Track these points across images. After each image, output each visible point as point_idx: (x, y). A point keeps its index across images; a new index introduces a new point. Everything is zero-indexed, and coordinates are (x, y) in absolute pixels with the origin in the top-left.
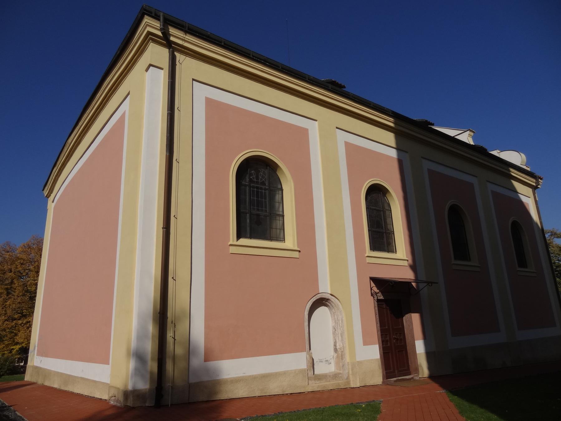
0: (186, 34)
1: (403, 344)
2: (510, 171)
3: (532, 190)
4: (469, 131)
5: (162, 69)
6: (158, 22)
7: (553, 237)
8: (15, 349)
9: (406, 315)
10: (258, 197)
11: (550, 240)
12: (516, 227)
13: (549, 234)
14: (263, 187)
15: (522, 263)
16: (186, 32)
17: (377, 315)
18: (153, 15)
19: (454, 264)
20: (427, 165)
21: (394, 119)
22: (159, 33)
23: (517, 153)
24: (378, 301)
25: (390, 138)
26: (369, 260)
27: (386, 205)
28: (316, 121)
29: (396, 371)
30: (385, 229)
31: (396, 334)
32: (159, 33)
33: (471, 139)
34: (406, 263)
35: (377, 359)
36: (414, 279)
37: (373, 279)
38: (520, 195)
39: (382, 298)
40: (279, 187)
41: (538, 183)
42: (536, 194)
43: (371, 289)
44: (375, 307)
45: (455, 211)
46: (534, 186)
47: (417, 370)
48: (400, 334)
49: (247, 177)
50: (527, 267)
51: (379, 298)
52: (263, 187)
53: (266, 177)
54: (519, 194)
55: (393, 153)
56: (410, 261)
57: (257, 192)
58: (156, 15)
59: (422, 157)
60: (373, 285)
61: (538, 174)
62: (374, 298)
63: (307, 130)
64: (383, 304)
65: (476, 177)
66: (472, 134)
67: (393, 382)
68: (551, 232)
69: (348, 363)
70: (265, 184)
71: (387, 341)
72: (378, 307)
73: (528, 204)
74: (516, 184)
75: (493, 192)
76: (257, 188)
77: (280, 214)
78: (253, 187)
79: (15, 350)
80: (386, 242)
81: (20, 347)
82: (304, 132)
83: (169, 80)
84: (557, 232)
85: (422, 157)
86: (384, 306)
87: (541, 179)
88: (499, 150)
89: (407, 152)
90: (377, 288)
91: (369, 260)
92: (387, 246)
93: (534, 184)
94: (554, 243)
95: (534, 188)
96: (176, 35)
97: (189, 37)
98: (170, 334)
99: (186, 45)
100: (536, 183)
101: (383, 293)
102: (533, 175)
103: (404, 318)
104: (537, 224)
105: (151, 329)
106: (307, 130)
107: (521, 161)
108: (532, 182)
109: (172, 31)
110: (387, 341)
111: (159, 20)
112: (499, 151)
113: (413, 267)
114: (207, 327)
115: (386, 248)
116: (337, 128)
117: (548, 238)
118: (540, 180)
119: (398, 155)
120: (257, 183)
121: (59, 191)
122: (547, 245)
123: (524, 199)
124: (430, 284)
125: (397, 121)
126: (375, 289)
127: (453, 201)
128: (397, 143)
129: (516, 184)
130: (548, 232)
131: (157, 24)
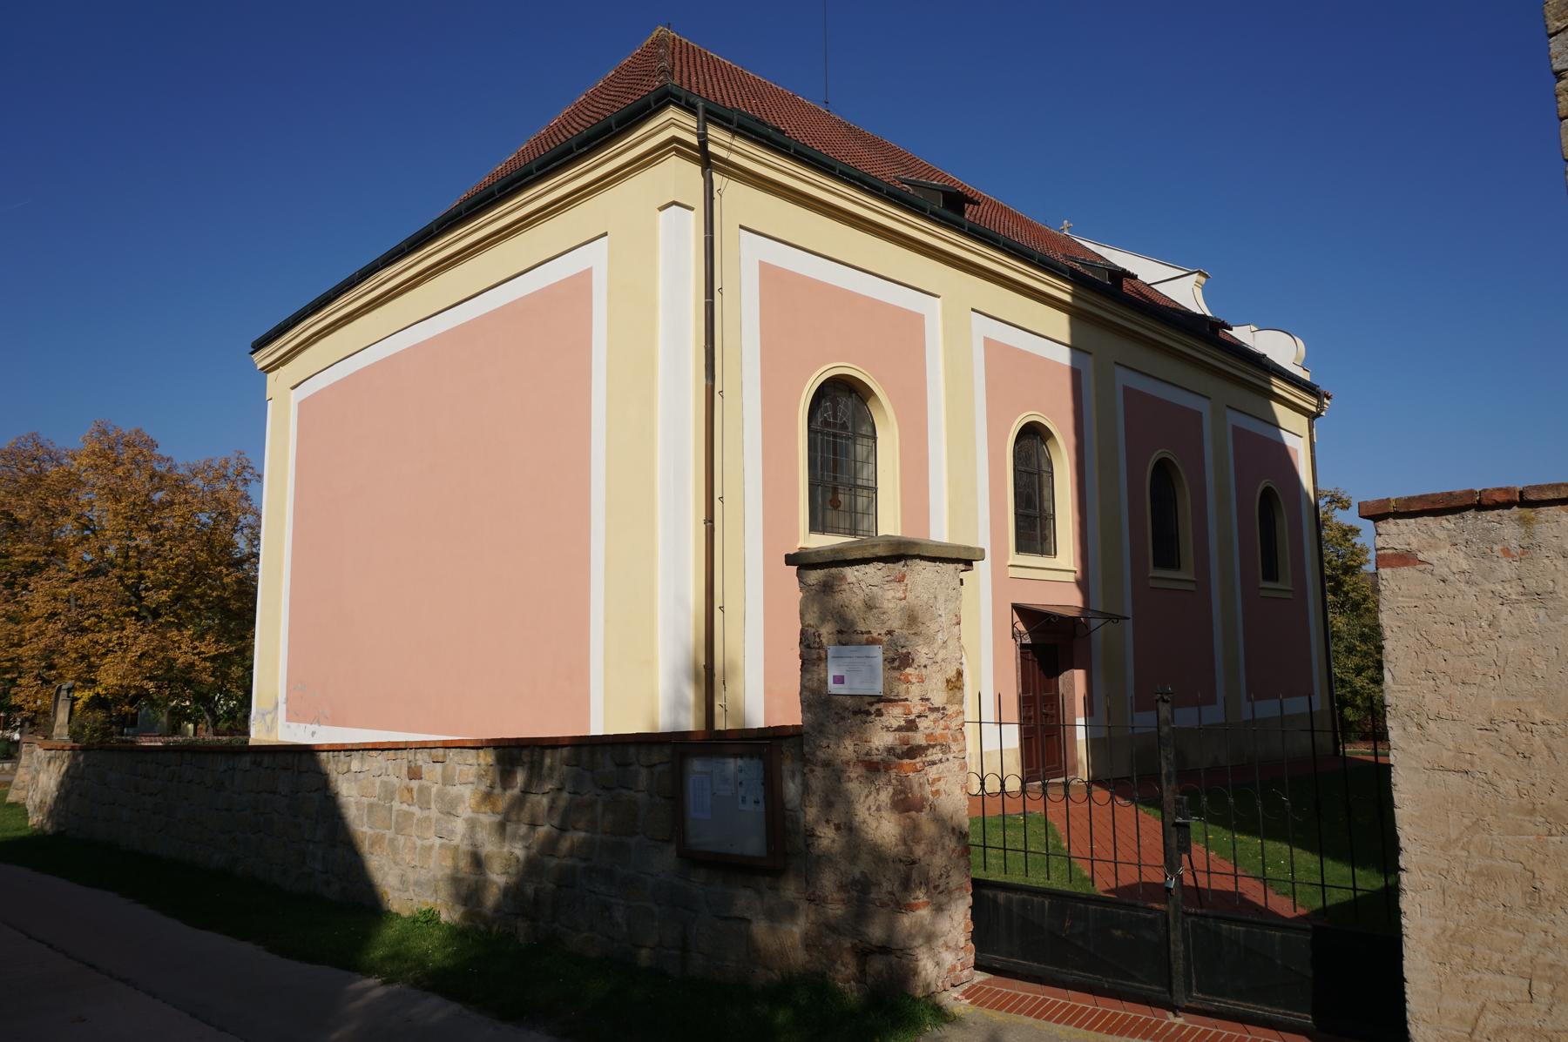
0: (733, 137)
1: (1054, 724)
2: (1270, 383)
3: (1309, 421)
4: (1196, 274)
5: (691, 209)
6: (695, 119)
7: (1333, 506)
8: (79, 699)
9: (1065, 673)
10: (835, 454)
11: (1326, 513)
12: (1268, 499)
13: (1328, 499)
14: (844, 433)
15: (1271, 573)
16: (735, 133)
17: (1020, 673)
18: (683, 103)
19: (1153, 578)
20: (1123, 378)
21: (1072, 286)
22: (694, 140)
23: (1289, 336)
24: (1023, 646)
25: (1059, 323)
26: (1013, 572)
27: (1043, 461)
28: (939, 297)
29: (1041, 770)
30: (1040, 510)
31: (1045, 706)
32: (694, 140)
33: (1200, 290)
34: (1071, 577)
35: (1016, 749)
36: (1081, 606)
37: (1017, 608)
38: (1282, 431)
39: (1028, 641)
40: (865, 429)
41: (1320, 406)
42: (1314, 430)
43: (1013, 626)
44: (1016, 658)
45: (1164, 473)
46: (1312, 412)
47: (1075, 769)
48: (1052, 705)
49: (819, 415)
50: (1276, 580)
51: (1024, 642)
52: (844, 433)
53: (849, 413)
54: (1282, 431)
55: (1063, 356)
56: (1079, 574)
57: (835, 443)
58: (687, 102)
59: (1116, 363)
60: (1016, 618)
61: (1323, 388)
62: (1016, 641)
63: (921, 317)
64: (1028, 653)
65: (1209, 398)
66: (1203, 280)
67: (1036, 788)
68: (1332, 496)
69: (970, 754)
70: (847, 428)
71: (1030, 718)
72: (1021, 657)
73: (1296, 451)
74: (1278, 408)
75: (1235, 428)
76: (835, 436)
77: (870, 485)
78: (828, 434)
79: (80, 702)
80: (1039, 536)
81: (91, 694)
82: (914, 323)
83: (706, 233)
84: (1343, 497)
85: (1116, 363)
86: (1030, 656)
87: (1328, 398)
88: (1255, 325)
89: (1090, 353)
90: (1391, 798)
91: (1013, 572)
92: (1042, 544)
93: (1313, 409)
94: (1334, 520)
95: (1312, 416)
96: (721, 142)
97: (739, 144)
98: (718, 702)
99: (734, 158)
100: (1317, 407)
101: (1031, 634)
102: (1314, 390)
103: (1060, 677)
104: (1308, 495)
105: (690, 694)
106: (921, 317)
107: (1294, 357)
108: (1310, 404)
109: (714, 132)
110: (1030, 718)
111: (695, 114)
112: (1254, 328)
113: (1083, 584)
114: (768, 692)
115: (1039, 547)
116: (973, 310)
117: (1325, 509)
118: (1326, 400)
119: (1073, 360)
120: (835, 425)
121: (325, 369)
122: (1319, 525)
123: (1289, 440)
124: (1115, 621)
125: (1077, 291)
126: (1021, 627)
127: (1163, 450)
128: (1073, 335)
129: (1278, 408)
130: (1326, 496)
131: (691, 122)
